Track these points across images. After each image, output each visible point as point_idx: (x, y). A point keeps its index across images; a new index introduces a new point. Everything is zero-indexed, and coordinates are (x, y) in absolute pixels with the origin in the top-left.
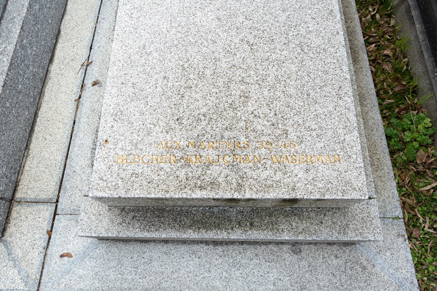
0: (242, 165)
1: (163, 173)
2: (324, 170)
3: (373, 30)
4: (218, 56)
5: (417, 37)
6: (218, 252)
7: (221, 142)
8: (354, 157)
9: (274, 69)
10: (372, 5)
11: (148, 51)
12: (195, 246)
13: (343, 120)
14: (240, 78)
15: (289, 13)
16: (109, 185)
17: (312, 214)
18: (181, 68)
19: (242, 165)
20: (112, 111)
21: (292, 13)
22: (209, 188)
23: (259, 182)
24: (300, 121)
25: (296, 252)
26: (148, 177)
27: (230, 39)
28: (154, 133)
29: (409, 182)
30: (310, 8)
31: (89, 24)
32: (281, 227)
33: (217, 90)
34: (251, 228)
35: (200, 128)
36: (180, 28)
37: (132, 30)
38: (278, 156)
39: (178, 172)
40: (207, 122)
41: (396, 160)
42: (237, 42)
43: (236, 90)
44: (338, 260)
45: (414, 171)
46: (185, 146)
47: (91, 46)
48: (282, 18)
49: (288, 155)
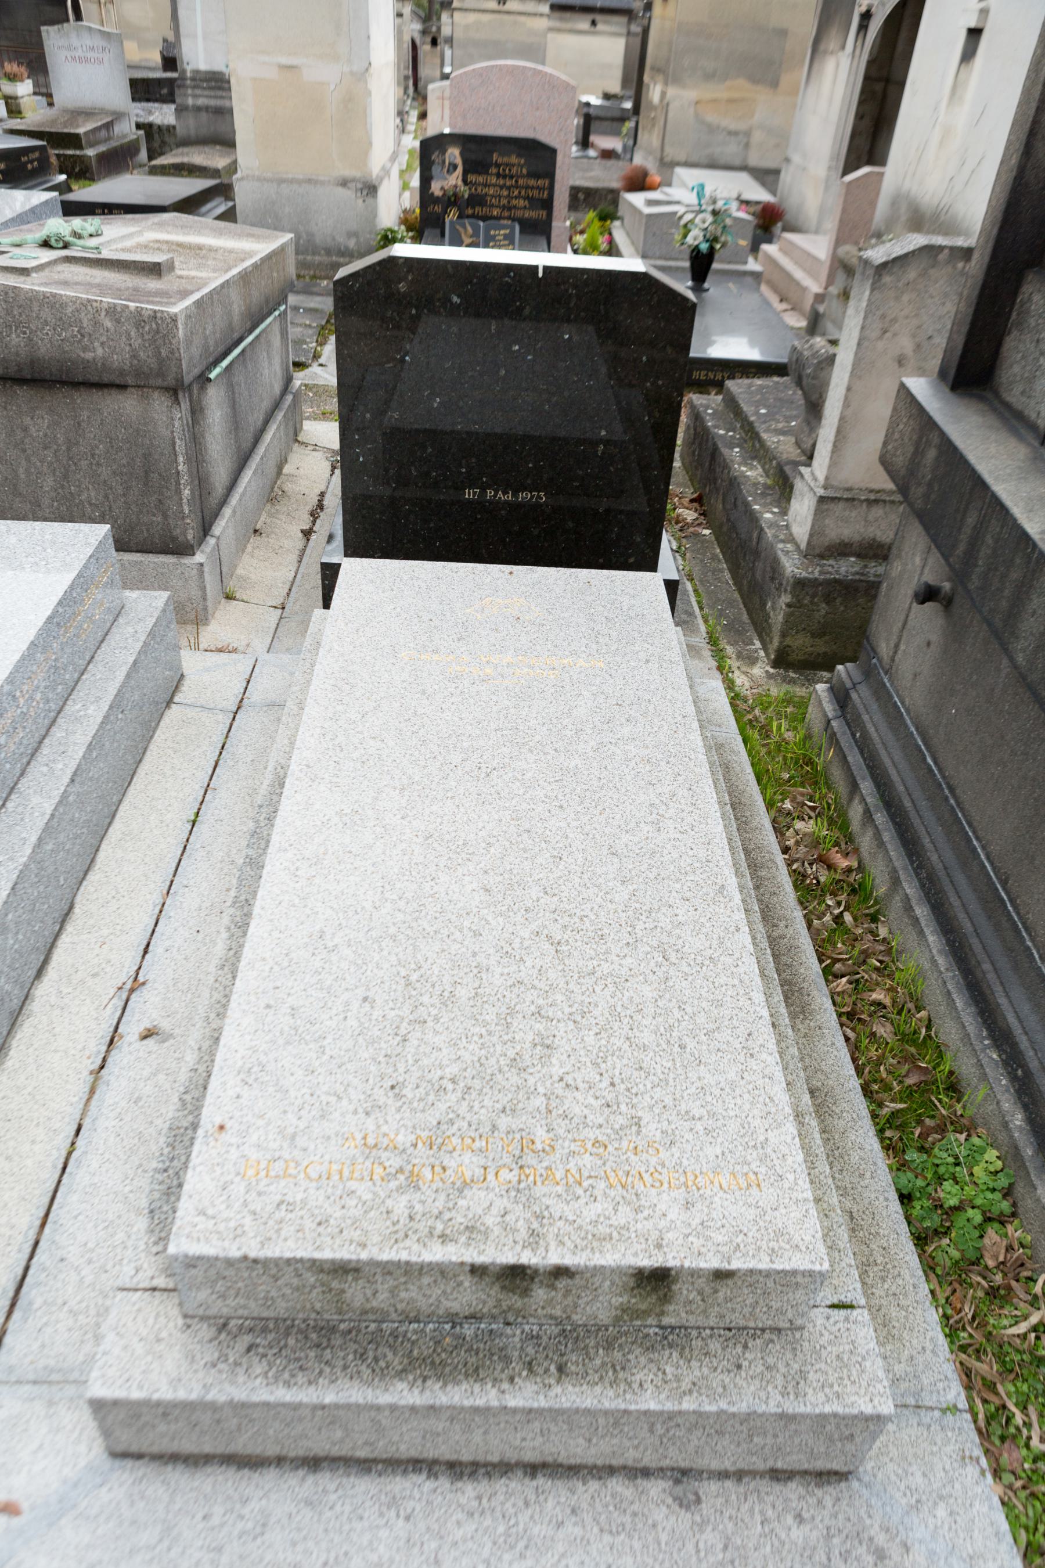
0: (539, 1190)
1: (354, 1202)
2: (726, 1203)
3: (839, 945)
4: (485, 962)
5: (933, 961)
6: (463, 1500)
7: (491, 1140)
8: (791, 1177)
9: (607, 992)
10: (834, 894)
11: (330, 944)
12: (398, 1479)
13: (761, 1099)
14: (533, 1008)
15: (635, 886)
16: (222, 1227)
17: (714, 1346)
18: (403, 981)
19: (539, 1190)
20: (240, 1063)
21: (642, 887)
22: (463, 1239)
23: (580, 1228)
24: (668, 1100)
25: (685, 1502)
26: (316, 1212)
27: (511, 930)
28: (337, 1114)
29: (974, 1318)
30: (678, 881)
31: (148, 896)
32: (638, 1377)
33: (483, 1031)
34: (560, 1377)
35: (442, 1106)
36: (402, 904)
37: (297, 901)
38: (620, 1173)
39: (389, 1203)
40: (459, 1095)
41: (933, 1258)
42: (527, 936)
43: (525, 1031)
44: (806, 1528)
45: (983, 1287)
46: (408, 1144)
47: (148, 945)
48: (622, 894)
49: (643, 1170)
